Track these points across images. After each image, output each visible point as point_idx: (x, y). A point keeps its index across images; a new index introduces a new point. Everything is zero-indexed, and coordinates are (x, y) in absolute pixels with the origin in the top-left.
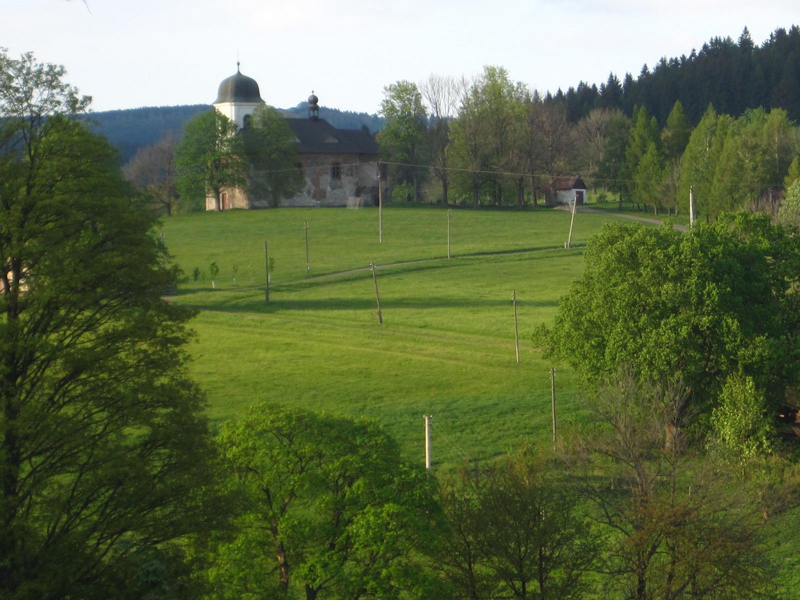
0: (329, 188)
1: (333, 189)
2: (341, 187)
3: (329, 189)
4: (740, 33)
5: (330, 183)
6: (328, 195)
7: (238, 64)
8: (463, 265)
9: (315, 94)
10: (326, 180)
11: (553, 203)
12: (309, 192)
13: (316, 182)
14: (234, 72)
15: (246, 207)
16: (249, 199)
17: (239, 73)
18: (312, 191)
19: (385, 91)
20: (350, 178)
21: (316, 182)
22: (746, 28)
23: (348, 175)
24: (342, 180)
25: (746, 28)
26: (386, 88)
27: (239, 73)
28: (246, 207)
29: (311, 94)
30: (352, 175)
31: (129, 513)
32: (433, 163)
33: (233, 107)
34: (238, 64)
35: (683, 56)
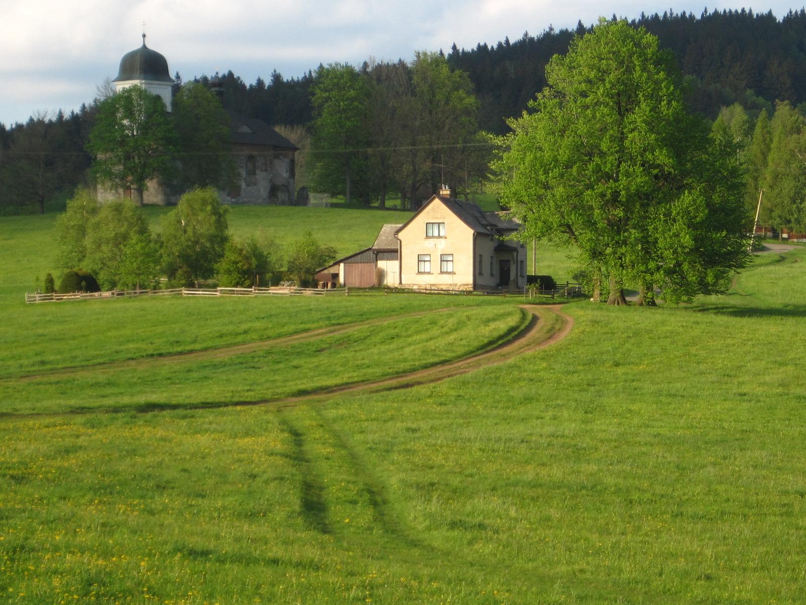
1: (248, 185)
2: (255, 184)
3: (244, 185)
4: (505, 39)
6: (242, 192)
7: (144, 36)
8: (228, 346)
11: (156, 288)
14: (138, 46)
15: (161, 203)
16: (165, 194)
17: (144, 46)
23: (262, 170)
25: (177, 74)
27: (144, 46)
28: (161, 203)
30: (266, 170)
32: (153, 192)
34: (144, 36)
35: (60, 113)
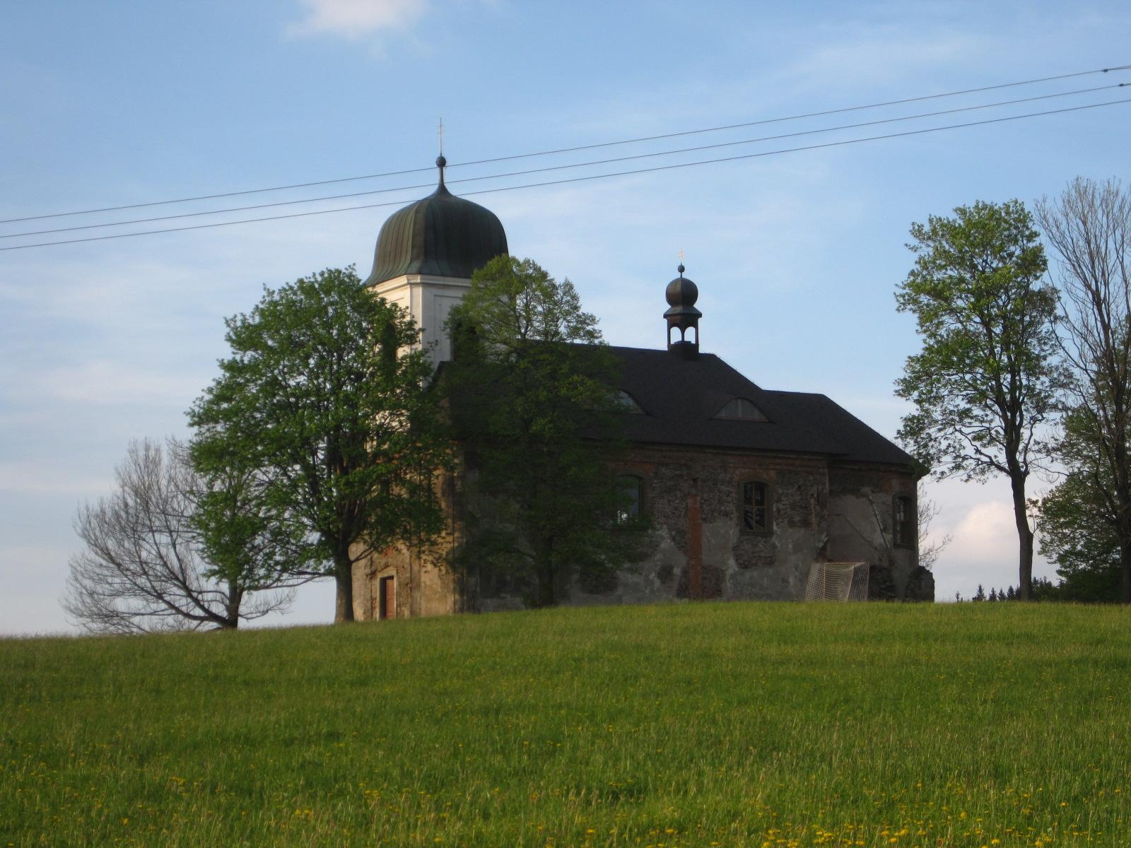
0: (732, 562)
1: (744, 566)
2: (770, 562)
3: (732, 565)
5: (735, 549)
9: (686, 275)
10: (722, 534)
12: (666, 573)
13: (689, 543)
17: (442, 189)
18: (677, 571)
19: (914, 242)
20: (800, 533)
21: (689, 543)
22: (980, 587)
23: (792, 524)
24: (775, 540)
25: (980, 587)
26: (918, 232)
27: (442, 189)
29: (678, 275)
30: (806, 523)
31: (582, 729)
33: (419, 291)
